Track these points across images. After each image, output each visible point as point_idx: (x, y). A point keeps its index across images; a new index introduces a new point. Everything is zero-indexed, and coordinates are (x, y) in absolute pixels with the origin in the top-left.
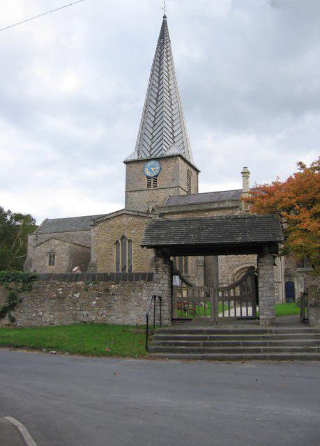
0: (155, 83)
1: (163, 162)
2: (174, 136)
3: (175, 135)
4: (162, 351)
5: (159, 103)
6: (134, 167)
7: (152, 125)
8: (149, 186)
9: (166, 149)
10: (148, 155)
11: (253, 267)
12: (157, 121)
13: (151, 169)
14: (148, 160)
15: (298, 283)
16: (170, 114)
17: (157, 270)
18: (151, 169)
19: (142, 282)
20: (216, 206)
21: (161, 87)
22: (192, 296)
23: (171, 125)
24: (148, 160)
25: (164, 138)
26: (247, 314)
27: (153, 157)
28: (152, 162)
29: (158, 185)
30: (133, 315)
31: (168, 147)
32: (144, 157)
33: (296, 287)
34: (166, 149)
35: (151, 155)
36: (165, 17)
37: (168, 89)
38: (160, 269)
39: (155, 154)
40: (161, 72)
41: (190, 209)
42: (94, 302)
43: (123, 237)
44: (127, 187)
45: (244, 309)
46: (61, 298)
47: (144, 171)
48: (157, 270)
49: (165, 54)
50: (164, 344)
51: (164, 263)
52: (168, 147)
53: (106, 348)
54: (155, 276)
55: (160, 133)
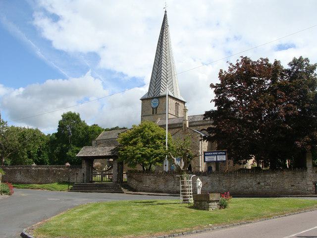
0: (153, 87)
1: (160, 100)
6: (147, 102)
7: (153, 92)
8: (153, 113)
10: (153, 95)
11: (215, 91)
12: (157, 83)
13: (153, 104)
14: (153, 98)
18: (153, 104)
22: (211, 199)
24: (153, 98)
27: (155, 96)
28: (155, 99)
30: (170, 187)
32: (151, 97)
35: (154, 95)
36: (166, 12)
44: (142, 113)
47: (151, 105)
53: (27, 181)
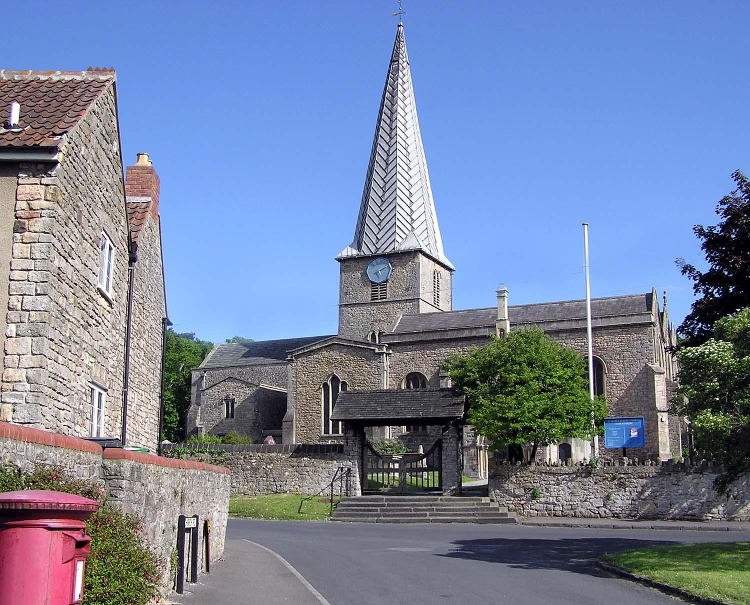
2: (412, 219)
3: (414, 216)
4: (344, 515)
5: (390, 167)
9: (400, 240)
15: (576, 445)
16: (407, 185)
17: (347, 442)
19: (333, 454)
20: (466, 334)
21: (393, 141)
23: (408, 202)
25: (398, 231)
26: (428, 486)
27: (380, 252)
29: (388, 296)
31: (404, 236)
33: (573, 451)
34: (400, 240)
37: (403, 144)
38: (350, 442)
39: (385, 246)
40: (395, 115)
41: (430, 337)
42: (287, 474)
43: (335, 379)
45: (375, 479)
46: (255, 470)
48: (347, 442)
49: (400, 88)
50: (347, 510)
51: (353, 436)
52: (404, 236)
54: (345, 449)
55: (392, 214)
